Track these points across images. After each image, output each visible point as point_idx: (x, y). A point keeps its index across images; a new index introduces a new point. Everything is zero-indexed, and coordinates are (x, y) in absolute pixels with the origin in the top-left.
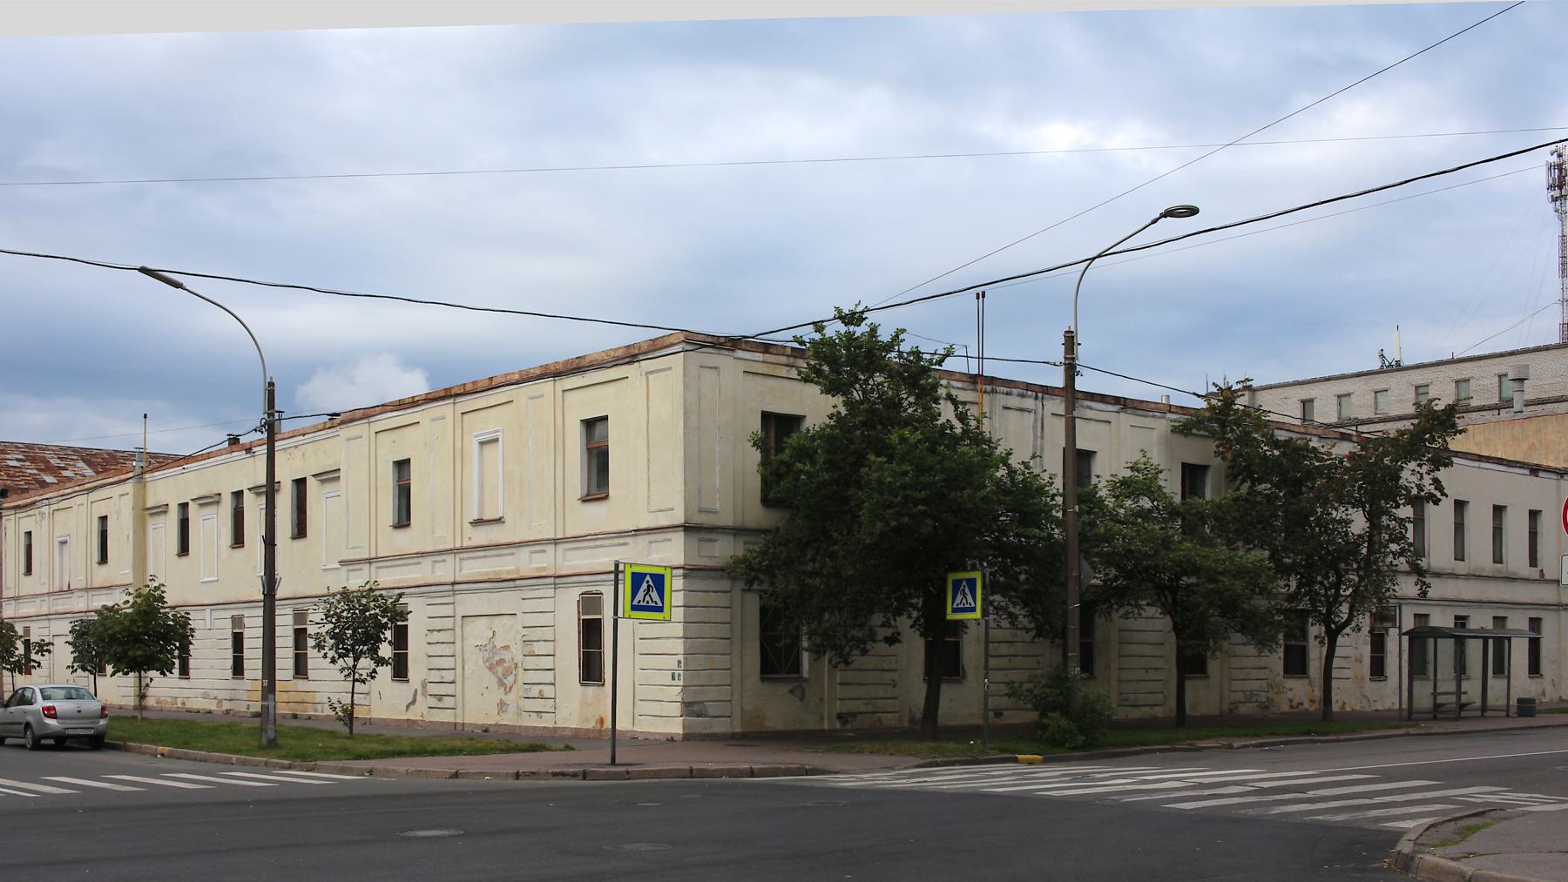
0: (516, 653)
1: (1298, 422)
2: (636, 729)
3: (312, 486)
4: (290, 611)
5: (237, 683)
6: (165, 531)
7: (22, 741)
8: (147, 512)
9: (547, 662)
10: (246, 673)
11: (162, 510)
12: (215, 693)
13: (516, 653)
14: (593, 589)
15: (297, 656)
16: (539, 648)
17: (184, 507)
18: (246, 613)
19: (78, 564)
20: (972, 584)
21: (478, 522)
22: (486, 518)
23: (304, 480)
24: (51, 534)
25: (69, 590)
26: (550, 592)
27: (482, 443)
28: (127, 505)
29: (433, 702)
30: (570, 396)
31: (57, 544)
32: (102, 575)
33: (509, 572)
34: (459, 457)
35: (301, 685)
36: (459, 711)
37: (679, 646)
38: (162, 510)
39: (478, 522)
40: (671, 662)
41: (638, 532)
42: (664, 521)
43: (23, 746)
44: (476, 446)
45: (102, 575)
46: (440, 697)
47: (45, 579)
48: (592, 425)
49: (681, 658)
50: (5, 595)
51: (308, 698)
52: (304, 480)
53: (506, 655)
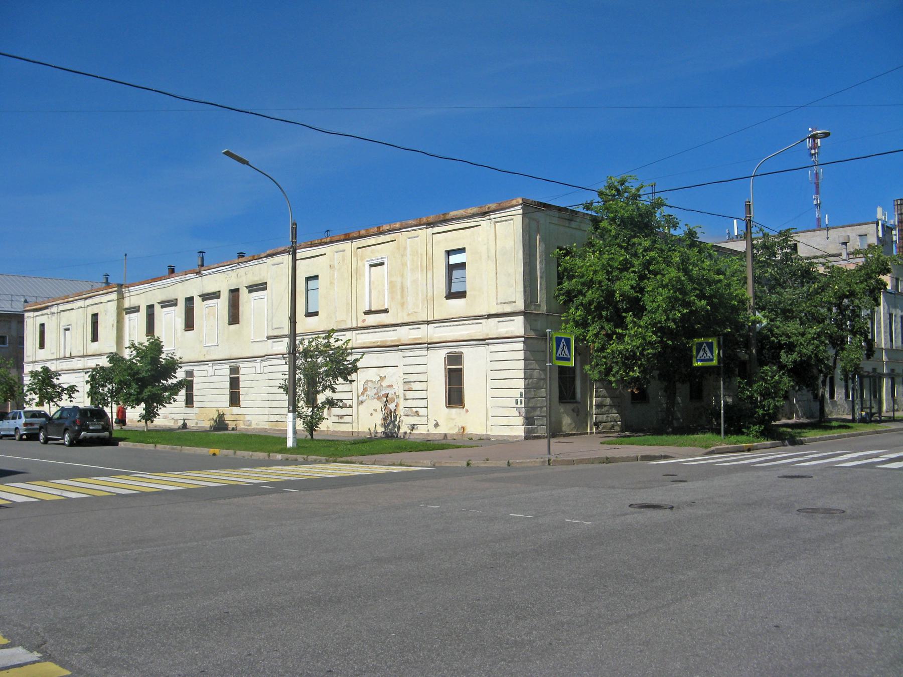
0: (399, 389)
1: (242, 365)
2: (489, 433)
3: (244, 294)
4: (227, 366)
5: (189, 410)
6: (177, 315)
7: (62, 441)
8: (123, 311)
9: (422, 394)
10: (195, 404)
11: (136, 309)
12: (173, 416)
13: (399, 389)
14: (457, 350)
15: (232, 393)
16: (415, 386)
17: (150, 308)
18: (195, 368)
19: (78, 341)
20: (710, 346)
21: (369, 312)
22: (373, 309)
23: (237, 290)
24: (58, 325)
25: (71, 357)
26: (424, 352)
27: (372, 266)
28: (113, 306)
29: (336, 419)
30: (498, 224)
31: (62, 331)
32: (94, 347)
33: (392, 341)
34: (355, 274)
35: (235, 410)
36: (355, 424)
37: (521, 384)
38: (136, 309)
39: (369, 312)
40: (516, 394)
41: (489, 316)
42: (508, 309)
43: (63, 444)
44: (367, 266)
45: (94, 347)
46: (341, 416)
47: (54, 350)
48: (42, 325)
49: (523, 390)
50: (26, 359)
51: (238, 417)
52: (237, 290)
53: (390, 392)
